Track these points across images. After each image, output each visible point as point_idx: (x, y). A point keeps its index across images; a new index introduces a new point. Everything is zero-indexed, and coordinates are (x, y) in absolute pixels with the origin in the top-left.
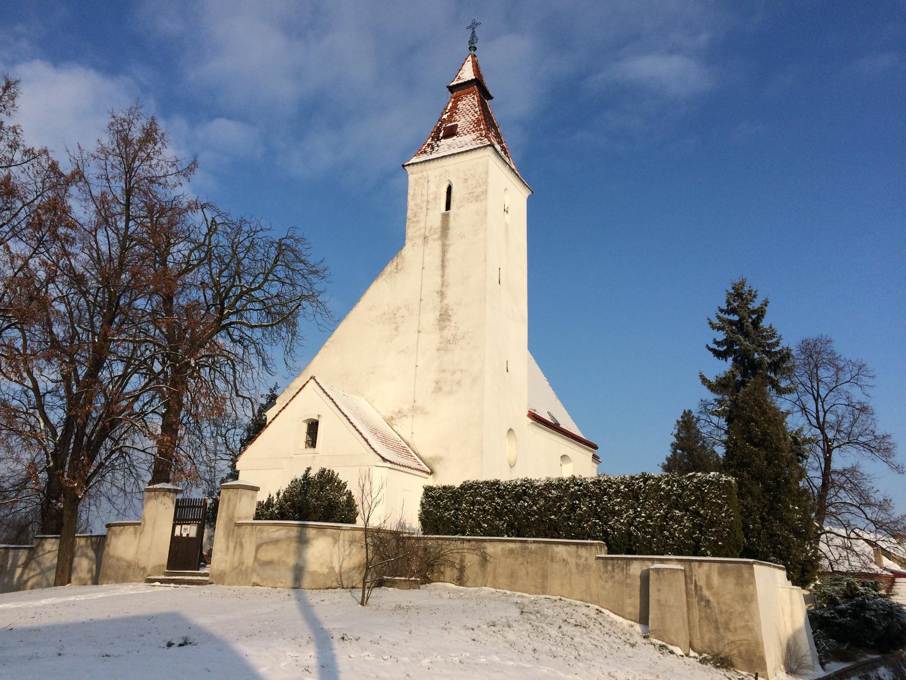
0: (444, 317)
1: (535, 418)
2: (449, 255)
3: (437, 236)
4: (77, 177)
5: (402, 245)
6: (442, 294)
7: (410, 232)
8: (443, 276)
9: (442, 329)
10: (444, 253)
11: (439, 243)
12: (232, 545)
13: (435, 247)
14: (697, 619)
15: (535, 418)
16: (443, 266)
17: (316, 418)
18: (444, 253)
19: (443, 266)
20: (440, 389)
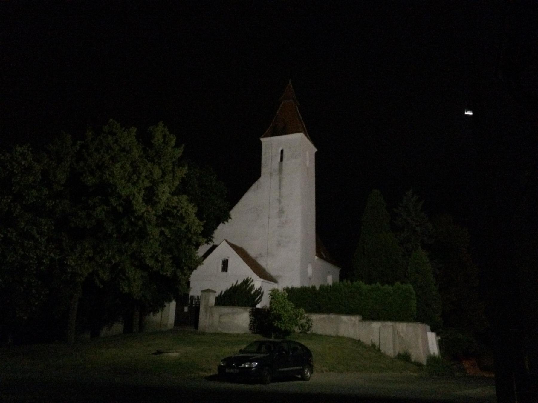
0: (281, 212)
1: (282, 151)
2: (284, 183)
3: (277, 173)
4: (134, 164)
5: (259, 176)
6: (280, 201)
7: (264, 170)
8: (280, 192)
9: (280, 217)
10: (280, 181)
11: (278, 177)
12: (208, 315)
13: (276, 178)
14: (176, 353)
15: (282, 151)
16: (280, 188)
17: (227, 258)
18: (280, 181)
19: (280, 188)
20: (280, 245)
